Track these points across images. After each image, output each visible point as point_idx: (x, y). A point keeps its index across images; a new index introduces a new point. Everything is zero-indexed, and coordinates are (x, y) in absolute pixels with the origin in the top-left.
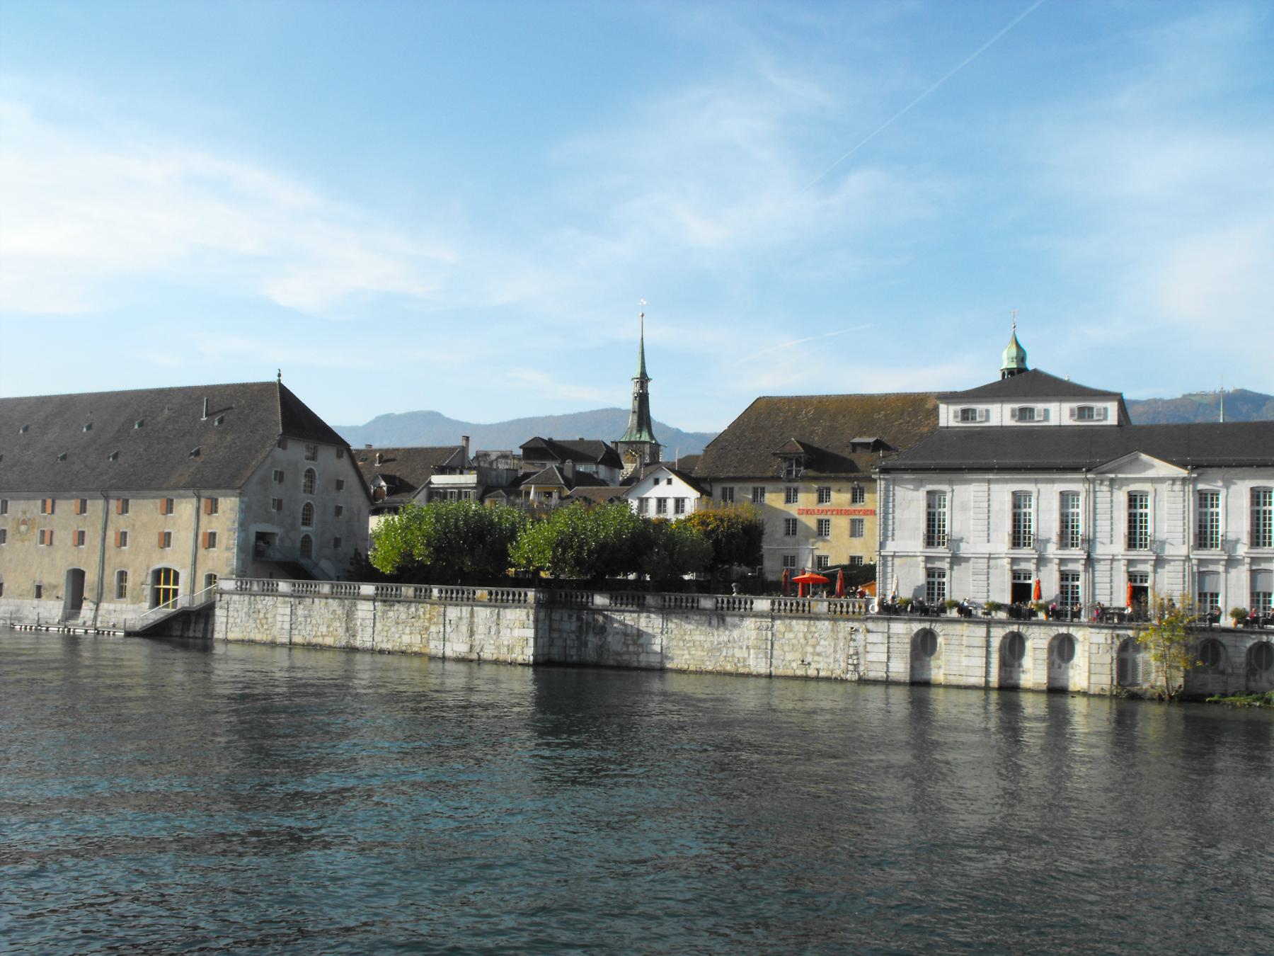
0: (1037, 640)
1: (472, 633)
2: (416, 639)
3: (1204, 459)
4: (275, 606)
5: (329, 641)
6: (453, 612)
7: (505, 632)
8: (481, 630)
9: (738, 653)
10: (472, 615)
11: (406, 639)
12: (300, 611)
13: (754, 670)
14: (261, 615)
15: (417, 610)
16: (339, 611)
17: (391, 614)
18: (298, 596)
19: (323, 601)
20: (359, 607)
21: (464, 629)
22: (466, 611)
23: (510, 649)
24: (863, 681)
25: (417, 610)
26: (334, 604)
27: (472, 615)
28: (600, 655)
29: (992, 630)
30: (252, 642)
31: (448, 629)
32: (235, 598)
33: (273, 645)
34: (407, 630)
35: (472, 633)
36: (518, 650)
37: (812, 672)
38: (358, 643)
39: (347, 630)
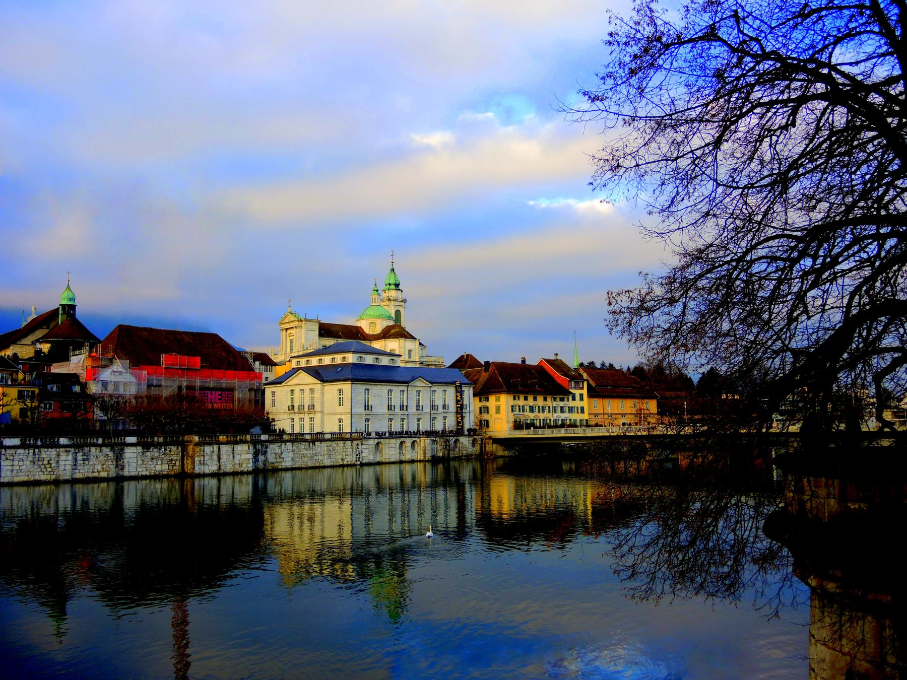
0: (307, 418)
1: (219, 459)
2: (165, 467)
3: (434, 380)
4: (58, 455)
5: (104, 474)
6: (208, 449)
7: (237, 457)
8: (224, 457)
9: (320, 458)
10: (219, 450)
11: (159, 468)
12: (80, 456)
13: (326, 464)
14: (46, 462)
15: (165, 450)
16: (111, 454)
17: (148, 454)
18: (78, 447)
19: (98, 449)
20: (126, 451)
21: (215, 457)
22: (216, 447)
23: (240, 465)
24: (362, 465)
25: (165, 450)
26: (106, 450)
27: (219, 450)
28: (265, 465)
29: (223, 481)
30: (38, 483)
31: (206, 458)
32: (21, 451)
33: (57, 483)
34: (159, 462)
35: (219, 459)
36: (244, 465)
37: (345, 463)
38: (126, 473)
39: (117, 466)
